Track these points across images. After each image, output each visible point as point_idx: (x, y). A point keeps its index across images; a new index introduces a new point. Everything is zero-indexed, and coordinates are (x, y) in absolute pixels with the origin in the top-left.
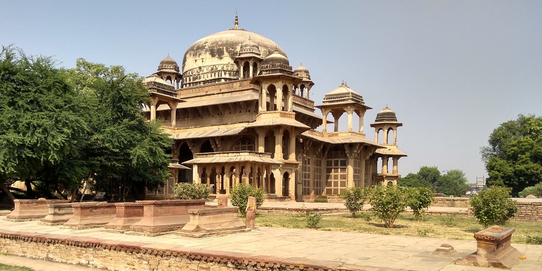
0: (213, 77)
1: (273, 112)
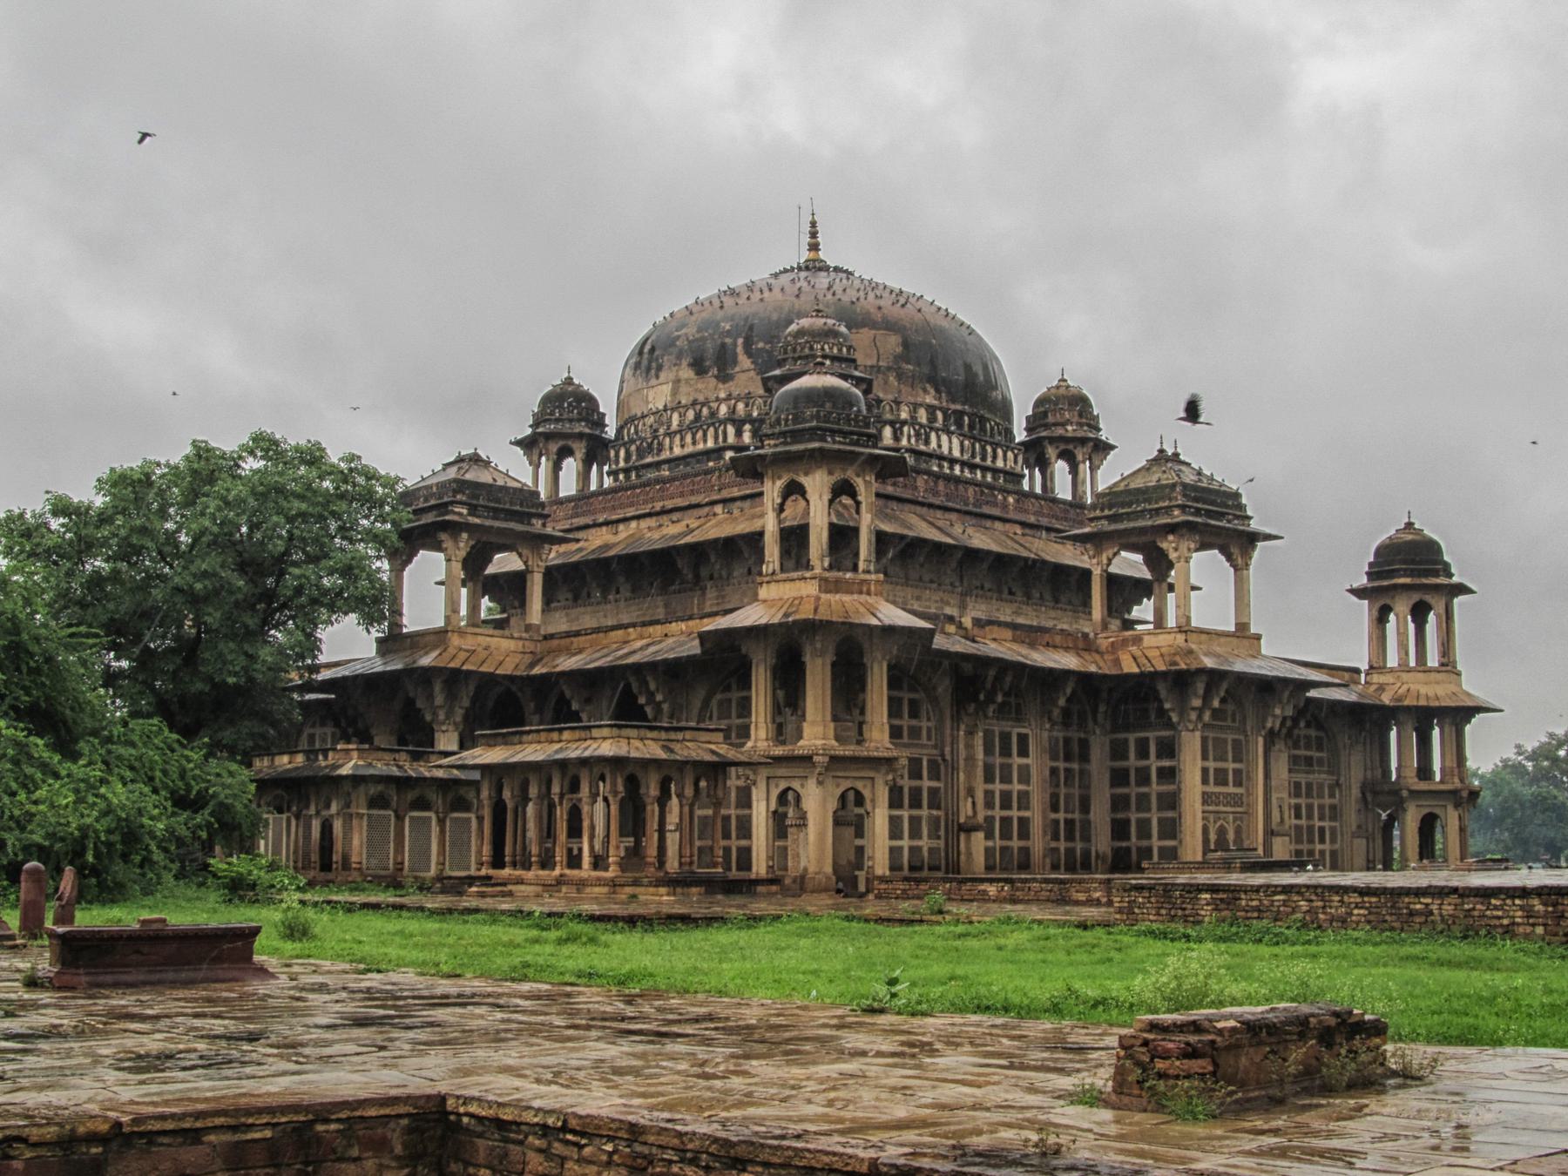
0: (701, 446)
1: (795, 575)
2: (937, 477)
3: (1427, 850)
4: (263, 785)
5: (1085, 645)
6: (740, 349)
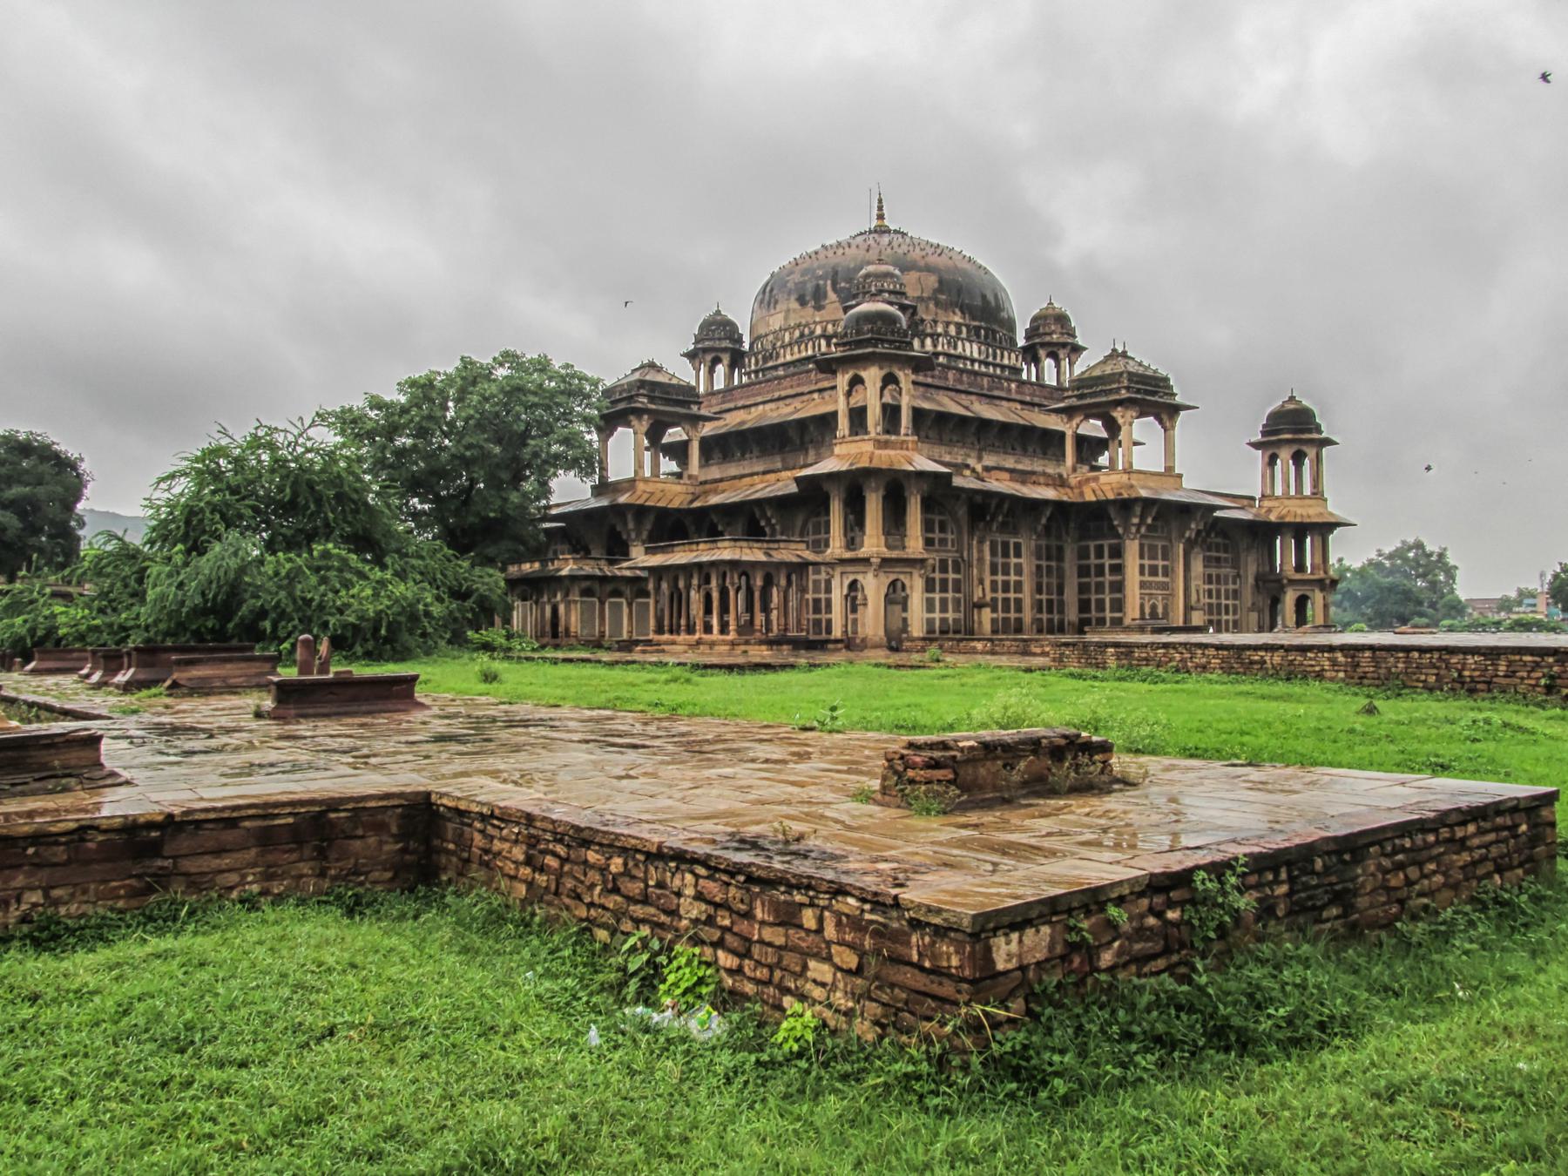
0: (804, 354)
2: (962, 371)
3: (1301, 620)
4: (512, 583)
5: (1060, 482)
6: (829, 288)
